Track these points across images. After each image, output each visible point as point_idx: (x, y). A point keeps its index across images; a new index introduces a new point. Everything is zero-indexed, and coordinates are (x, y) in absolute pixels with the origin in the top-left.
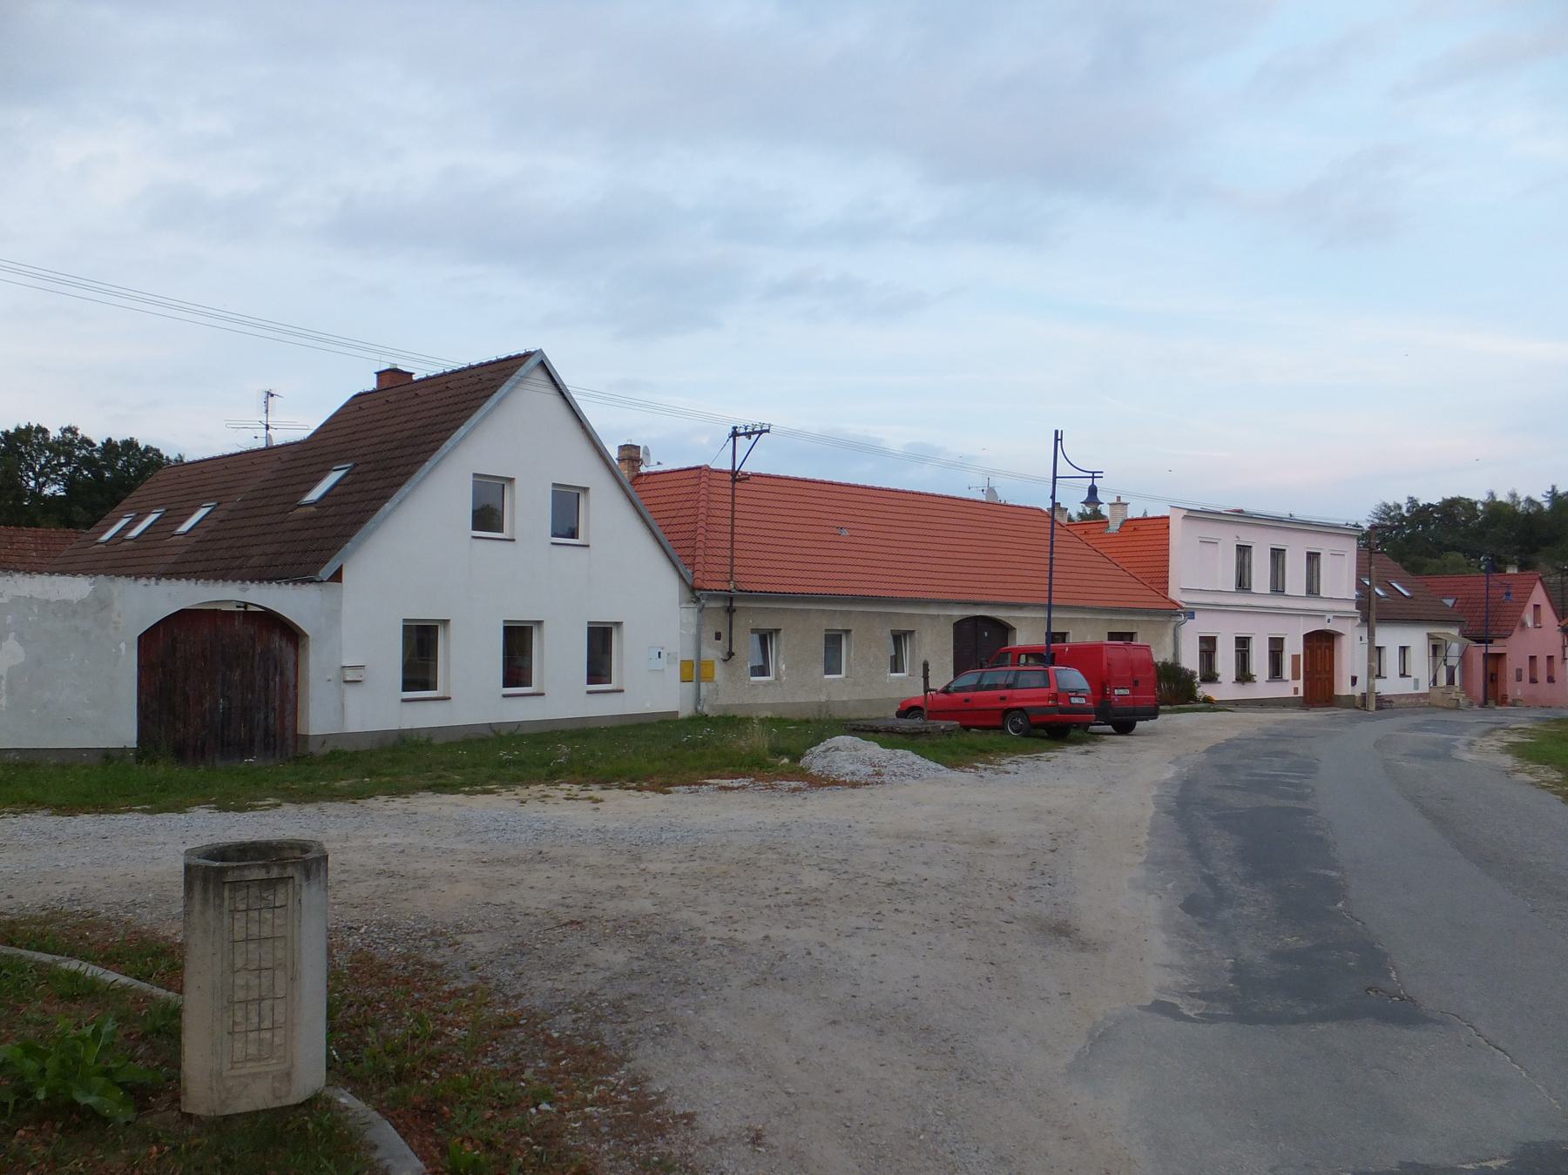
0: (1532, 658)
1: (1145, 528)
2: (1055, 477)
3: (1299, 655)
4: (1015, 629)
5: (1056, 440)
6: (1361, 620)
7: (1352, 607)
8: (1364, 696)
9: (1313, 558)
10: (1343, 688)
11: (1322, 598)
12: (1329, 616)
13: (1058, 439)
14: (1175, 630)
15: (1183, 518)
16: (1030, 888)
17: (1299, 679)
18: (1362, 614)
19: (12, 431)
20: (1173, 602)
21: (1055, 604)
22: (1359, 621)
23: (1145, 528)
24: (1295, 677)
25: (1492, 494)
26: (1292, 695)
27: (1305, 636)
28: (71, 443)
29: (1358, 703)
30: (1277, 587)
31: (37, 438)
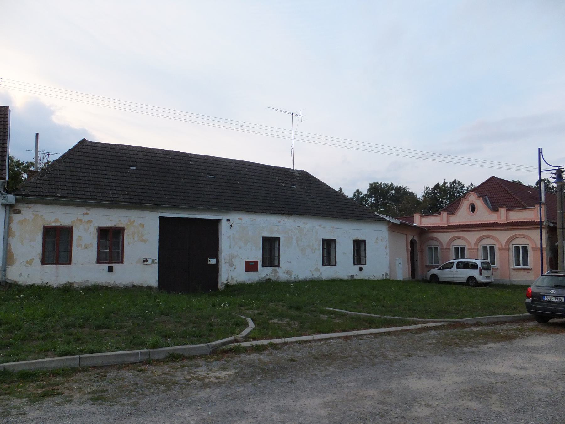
2: (540, 171)
16: (562, 374)
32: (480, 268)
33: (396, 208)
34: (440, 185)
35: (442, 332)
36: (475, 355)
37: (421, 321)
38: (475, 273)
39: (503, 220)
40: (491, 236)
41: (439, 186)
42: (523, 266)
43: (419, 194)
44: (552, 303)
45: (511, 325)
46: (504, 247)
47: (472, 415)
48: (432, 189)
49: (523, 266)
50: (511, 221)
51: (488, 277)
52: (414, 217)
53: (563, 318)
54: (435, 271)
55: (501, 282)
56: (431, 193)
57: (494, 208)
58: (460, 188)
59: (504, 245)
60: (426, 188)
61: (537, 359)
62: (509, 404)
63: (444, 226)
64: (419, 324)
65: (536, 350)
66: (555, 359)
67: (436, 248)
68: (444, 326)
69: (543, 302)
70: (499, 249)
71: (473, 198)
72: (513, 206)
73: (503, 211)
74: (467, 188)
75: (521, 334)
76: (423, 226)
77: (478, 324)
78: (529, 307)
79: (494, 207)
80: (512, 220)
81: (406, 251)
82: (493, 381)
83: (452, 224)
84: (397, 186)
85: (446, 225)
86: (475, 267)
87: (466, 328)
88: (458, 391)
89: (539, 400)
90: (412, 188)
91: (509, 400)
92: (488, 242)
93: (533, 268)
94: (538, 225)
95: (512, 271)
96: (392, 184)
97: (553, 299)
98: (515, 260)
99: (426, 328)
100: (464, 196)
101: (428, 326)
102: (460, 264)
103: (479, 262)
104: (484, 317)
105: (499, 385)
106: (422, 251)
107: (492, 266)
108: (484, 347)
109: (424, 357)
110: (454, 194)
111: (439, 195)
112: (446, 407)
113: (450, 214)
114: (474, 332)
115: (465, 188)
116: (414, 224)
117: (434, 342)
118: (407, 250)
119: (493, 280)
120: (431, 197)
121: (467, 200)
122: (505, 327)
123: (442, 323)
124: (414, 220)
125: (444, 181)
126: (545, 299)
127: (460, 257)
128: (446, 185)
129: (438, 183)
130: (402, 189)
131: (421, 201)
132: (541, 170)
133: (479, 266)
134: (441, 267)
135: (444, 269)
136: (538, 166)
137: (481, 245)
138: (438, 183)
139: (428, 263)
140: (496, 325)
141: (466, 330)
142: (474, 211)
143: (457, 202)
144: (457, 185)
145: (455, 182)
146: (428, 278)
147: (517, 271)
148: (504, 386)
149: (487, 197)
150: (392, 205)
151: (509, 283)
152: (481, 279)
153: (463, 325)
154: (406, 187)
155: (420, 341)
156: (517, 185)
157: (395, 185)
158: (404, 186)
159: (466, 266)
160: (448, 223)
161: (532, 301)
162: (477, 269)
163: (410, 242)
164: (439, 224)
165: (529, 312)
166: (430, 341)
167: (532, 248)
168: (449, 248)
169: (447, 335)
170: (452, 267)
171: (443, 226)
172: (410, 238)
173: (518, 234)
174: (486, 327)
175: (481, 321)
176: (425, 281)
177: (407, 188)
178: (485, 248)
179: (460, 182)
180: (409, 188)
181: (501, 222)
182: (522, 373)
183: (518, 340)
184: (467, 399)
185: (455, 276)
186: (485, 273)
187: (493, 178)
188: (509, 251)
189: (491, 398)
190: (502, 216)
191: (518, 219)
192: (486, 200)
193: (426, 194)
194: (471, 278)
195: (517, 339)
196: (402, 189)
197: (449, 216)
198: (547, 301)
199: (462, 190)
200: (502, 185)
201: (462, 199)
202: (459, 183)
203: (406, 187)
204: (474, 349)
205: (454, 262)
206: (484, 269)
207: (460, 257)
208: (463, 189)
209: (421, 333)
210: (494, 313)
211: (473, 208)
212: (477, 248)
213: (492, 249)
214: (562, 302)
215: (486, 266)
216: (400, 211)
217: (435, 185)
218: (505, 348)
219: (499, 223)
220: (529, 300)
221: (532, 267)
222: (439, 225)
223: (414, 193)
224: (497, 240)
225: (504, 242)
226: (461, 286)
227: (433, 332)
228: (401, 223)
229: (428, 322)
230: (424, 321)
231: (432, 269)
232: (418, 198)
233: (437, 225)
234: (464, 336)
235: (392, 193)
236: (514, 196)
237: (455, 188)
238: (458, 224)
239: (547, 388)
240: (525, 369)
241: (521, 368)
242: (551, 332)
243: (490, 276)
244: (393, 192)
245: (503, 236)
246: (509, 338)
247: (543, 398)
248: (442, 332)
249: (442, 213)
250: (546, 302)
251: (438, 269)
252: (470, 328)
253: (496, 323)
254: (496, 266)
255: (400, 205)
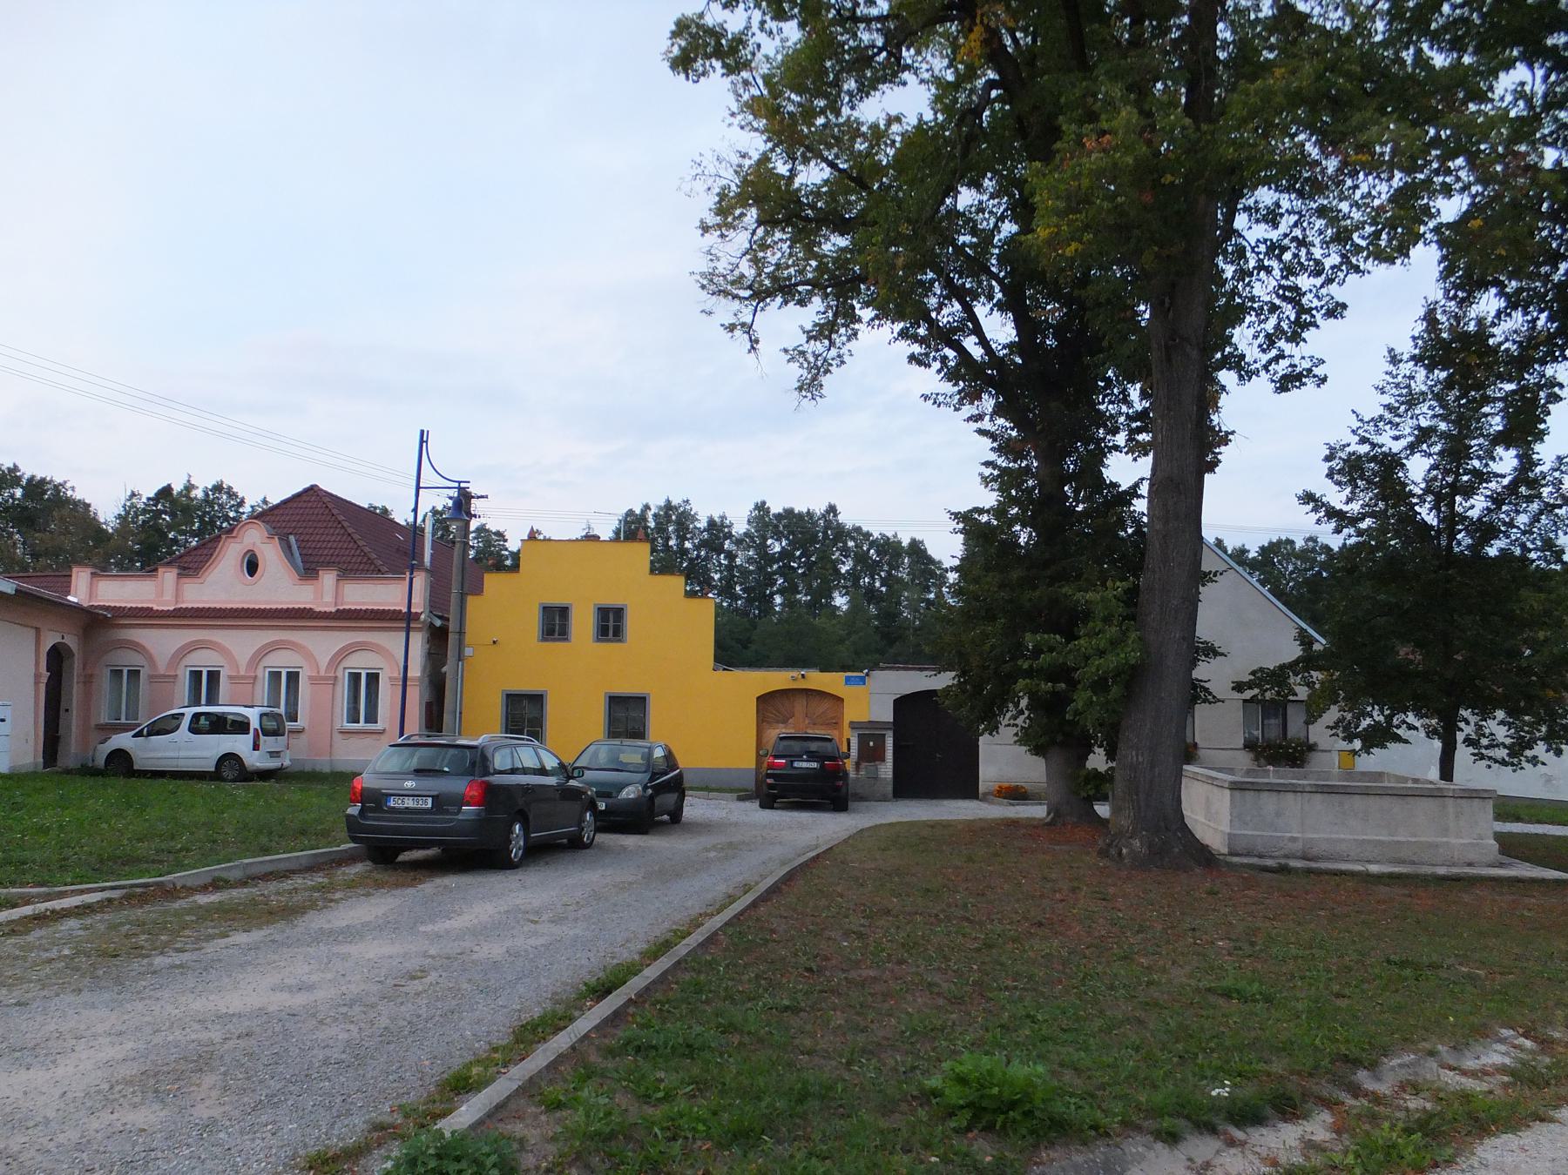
2: (418, 488)
5: (422, 442)
16: (395, 985)
19: (1266, 545)
21: (393, 641)
25: (832, 509)
28: (1313, 550)
31: (1285, 548)
32: (256, 730)
33: (24, 543)
34: (175, 492)
35: (100, 921)
36: (182, 974)
37: (39, 895)
38: (239, 744)
39: (326, 604)
40: (294, 643)
41: (172, 494)
42: (366, 722)
43: (107, 511)
44: (405, 813)
45: (304, 878)
46: (322, 673)
47: (128, 1147)
48: (149, 499)
49: (366, 722)
50: (347, 607)
51: (274, 754)
52: (71, 576)
53: (428, 848)
54: (123, 740)
55: (308, 768)
56: (144, 511)
57: (309, 570)
58: (233, 506)
59: (324, 668)
60: (129, 493)
61: (345, 957)
62: (245, 1090)
63: (165, 608)
64: (27, 903)
65: (351, 934)
66: (387, 949)
67: (134, 674)
68: (110, 900)
69: (387, 812)
70: (310, 678)
71: (255, 538)
72: (356, 567)
73: (328, 578)
74: (250, 509)
75: (323, 898)
76: (97, 607)
77: (216, 884)
78: (353, 827)
79: (308, 565)
80: (349, 603)
81: (32, 680)
82: (216, 1036)
83: (190, 606)
84: (33, 477)
85: (172, 608)
86: (241, 727)
87: (180, 898)
88: (106, 1086)
89: (326, 1062)
90: (81, 491)
91: (248, 1079)
92: (283, 661)
93: (306, 728)
94: (404, 620)
95: (338, 737)
96: (16, 468)
97: (409, 803)
98: (348, 709)
99: (48, 913)
100: (233, 527)
101: (58, 907)
102: (203, 718)
103: (253, 715)
104: (236, 863)
105: (231, 1044)
106: (88, 680)
107: (289, 725)
108: (211, 948)
109: (18, 1004)
110: (212, 522)
111: (168, 518)
112: (51, 1146)
113: (187, 576)
114: (200, 907)
115: (247, 509)
116: (69, 598)
117: (66, 952)
118: (37, 676)
119: (287, 763)
120: (144, 521)
121: (238, 540)
122: (287, 885)
123: (107, 894)
124: (70, 587)
125: (189, 481)
126: (392, 804)
127: (203, 701)
128: (193, 494)
129: (169, 485)
130: (49, 486)
131: (110, 531)
132: (421, 485)
133: (255, 724)
134: (143, 729)
135: (150, 734)
136: (415, 474)
137: (345, 668)
138: (169, 485)
139: (104, 719)
140: (267, 881)
141: (177, 905)
142: (255, 572)
143: (210, 545)
144: (225, 497)
145: (218, 488)
146: (101, 761)
147: (349, 735)
148: (242, 1043)
149: (292, 539)
150: (8, 533)
151: (327, 769)
152: (255, 760)
153: (170, 893)
154: (65, 482)
155: (17, 958)
156: (378, 519)
157: (28, 470)
158: (58, 480)
159: (219, 725)
160: (336, 604)
161: (362, 811)
162: (248, 733)
163: (48, 653)
164: (150, 601)
165: (354, 840)
166: (53, 954)
167: (390, 678)
168: (173, 673)
169: (113, 927)
170: (177, 727)
171: (160, 608)
172: (50, 640)
173: (273, 642)
174: (237, 890)
175: (224, 875)
176: (88, 771)
177: (68, 485)
178: (275, 676)
179: (235, 490)
180: (73, 489)
181: (323, 609)
182: (300, 1000)
183: (311, 914)
184: (125, 1104)
185: (182, 754)
186: (268, 743)
187: (313, 490)
188: (334, 685)
189: (199, 1085)
190: (325, 592)
191: (364, 603)
192: (290, 547)
193: (128, 513)
194: (230, 758)
195: (312, 912)
196: (49, 486)
197: (341, 583)
198: (394, 808)
199: (237, 512)
200: (335, 511)
201: (224, 537)
202: (231, 494)
203: (65, 482)
204: (186, 957)
205: (183, 714)
206: (267, 733)
207: (203, 701)
208: (241, 510)
209: (27, 932)
210: (266, 851)
211: (252, 567)
212: (253, 674)
213: (293, 677)
214: (428, 809)
215: (272, 725)
216: (35, 556)
217: (160, 487)
218: (273, 941)
219: (318, 610)
220: (354, 810)
221: (386, 726)
222: (150, 606)
223: (89, 505)
224: (309, 656)
225: (324, 661)
226: (195, 781)
227: (72, 923)
228: (16, 590)
229: (62, 895)
230: (49, 894)
231: (114, 736)
232: (102, 520)
233: (145, 605)
234: (166, 922)
235: (12, 496)
236: (361, 543)
237: (219, 505)
238: (207, 606)
239: (352, 1027)
240: (310, 988)
241: (302, 988)
242: (397, 885)
243: (277, 752)
244: (18, 493)
245: (322, 646)
246: (289, 912)
247: (336, 1056)
248: (100, 921)
249: (161, 570)
250: (394, 810)
251: (133, 736)
252: (191, 899)
253: (267, 877)
254: (300, 723)
255: (37, 535)
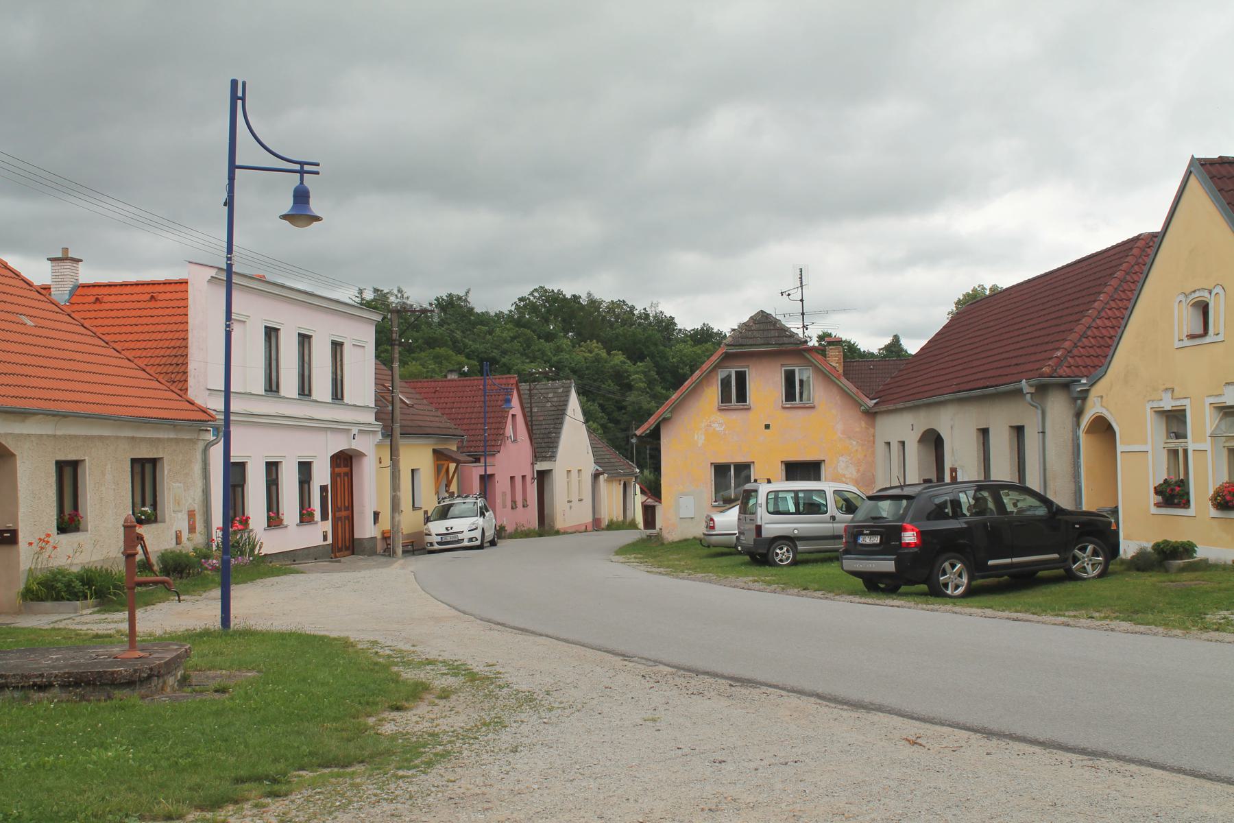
0: (512, 478)
1: (168, 296)
2: (233, 167)
3: (327, 485)
4: (13, 455)
5: (234, 98)
6: (383, 435)
7: (370, 418)
8: (385, 537)
9: (337, 346)
10: (366, 529)
11: (284, 398)
12: (355, 430)
13: (237, 95)
14: (206, 447)
15: (209, 281)
17: (327, 519)
18: (384, 427)
20: (204, 411)
22: (379, 436)
23: (168, 296)
24: (324, 517)
26: (321, 543)
27: (332, 458)
29: (380, 546)
30: (305, 390)
